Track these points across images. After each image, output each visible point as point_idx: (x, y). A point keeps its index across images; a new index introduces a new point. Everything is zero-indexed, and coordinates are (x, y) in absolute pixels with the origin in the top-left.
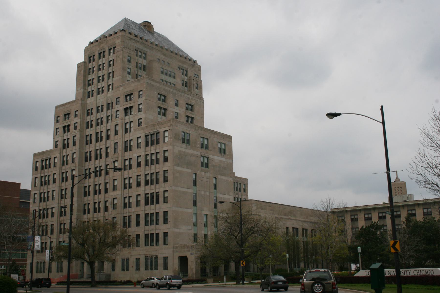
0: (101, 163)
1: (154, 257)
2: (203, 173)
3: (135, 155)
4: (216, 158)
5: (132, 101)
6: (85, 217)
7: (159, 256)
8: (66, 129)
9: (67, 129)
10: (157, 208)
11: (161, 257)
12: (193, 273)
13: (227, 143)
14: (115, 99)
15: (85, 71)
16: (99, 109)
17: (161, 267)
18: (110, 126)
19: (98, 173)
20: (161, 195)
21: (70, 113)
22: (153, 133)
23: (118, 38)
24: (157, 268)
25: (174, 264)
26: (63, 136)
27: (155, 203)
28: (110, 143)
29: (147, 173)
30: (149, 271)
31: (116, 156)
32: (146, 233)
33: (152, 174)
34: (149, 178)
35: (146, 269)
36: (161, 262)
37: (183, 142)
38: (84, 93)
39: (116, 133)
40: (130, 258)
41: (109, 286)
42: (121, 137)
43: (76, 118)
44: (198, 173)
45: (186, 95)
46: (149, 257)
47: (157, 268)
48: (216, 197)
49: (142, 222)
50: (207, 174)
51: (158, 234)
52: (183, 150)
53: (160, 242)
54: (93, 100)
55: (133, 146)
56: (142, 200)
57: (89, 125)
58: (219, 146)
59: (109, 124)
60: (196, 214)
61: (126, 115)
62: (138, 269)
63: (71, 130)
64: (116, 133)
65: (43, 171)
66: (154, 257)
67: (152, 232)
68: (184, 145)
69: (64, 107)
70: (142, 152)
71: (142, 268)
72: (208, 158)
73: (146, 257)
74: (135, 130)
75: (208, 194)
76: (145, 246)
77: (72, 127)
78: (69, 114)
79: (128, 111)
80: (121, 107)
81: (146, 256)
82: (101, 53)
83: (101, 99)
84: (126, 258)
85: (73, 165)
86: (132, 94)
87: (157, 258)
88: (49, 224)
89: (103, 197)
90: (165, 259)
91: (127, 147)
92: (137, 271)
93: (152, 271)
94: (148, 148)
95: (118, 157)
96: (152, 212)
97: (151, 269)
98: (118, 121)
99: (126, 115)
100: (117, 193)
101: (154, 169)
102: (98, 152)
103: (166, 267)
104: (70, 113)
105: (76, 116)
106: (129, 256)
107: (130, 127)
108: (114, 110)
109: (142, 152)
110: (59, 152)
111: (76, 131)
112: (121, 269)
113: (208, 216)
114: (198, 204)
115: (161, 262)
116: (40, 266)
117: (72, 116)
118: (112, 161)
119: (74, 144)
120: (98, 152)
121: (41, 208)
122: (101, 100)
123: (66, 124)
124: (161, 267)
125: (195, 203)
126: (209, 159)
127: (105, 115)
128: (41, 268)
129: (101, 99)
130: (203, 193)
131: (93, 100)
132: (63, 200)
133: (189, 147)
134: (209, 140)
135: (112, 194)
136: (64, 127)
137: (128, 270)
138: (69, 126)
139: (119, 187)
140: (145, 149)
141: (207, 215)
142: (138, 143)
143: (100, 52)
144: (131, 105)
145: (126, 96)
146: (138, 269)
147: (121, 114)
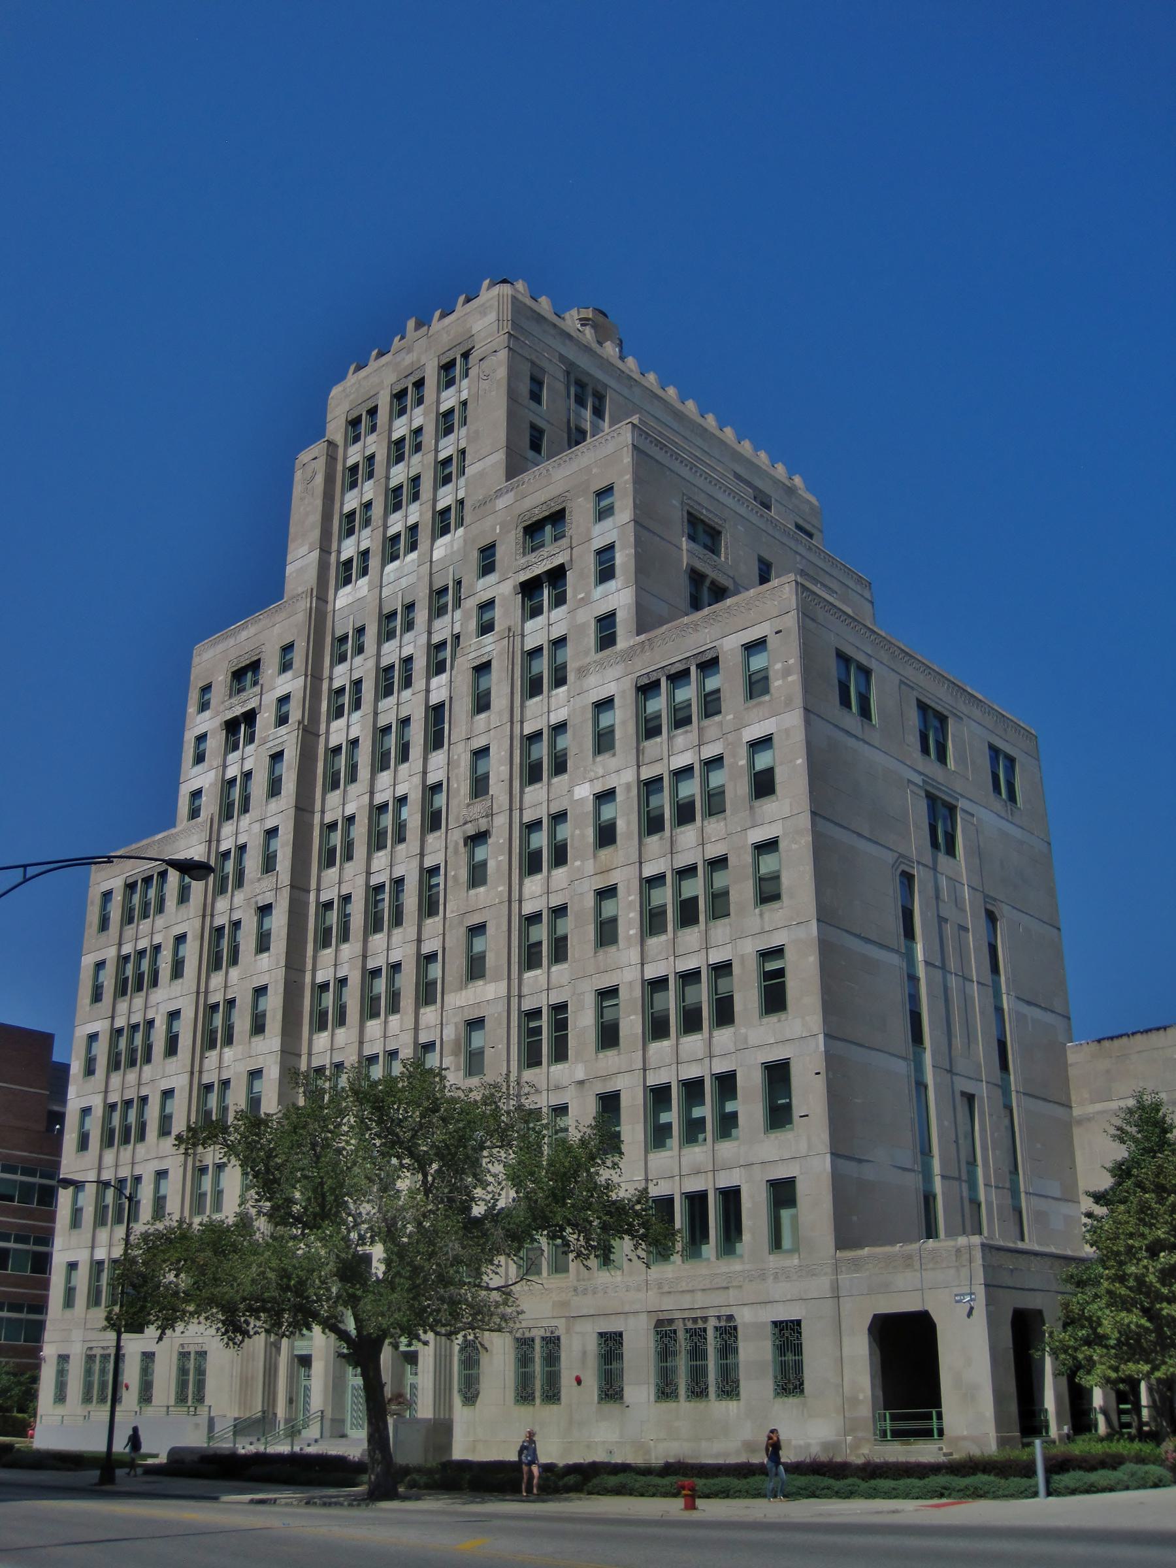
0: (400, 861)
1: (712, 1324)
3: (584, 792)
5: (564, 542)
6: (325, 1047)
7: (745, 1317)
10: (717, 1050)
15: (329, 479)
16: (391, 623)
17: (756, 1382)
19: (383, 905)
22: (680, 667)
24: (729, 1388)
25: (845, 1368)
26: (225, 767)
27: (702, 918)
29: (649, 871)
30: (684, 1406)
31: (480, 807)
32: (654, 1080)
33: (690, 977)
34: (670, 1001)
35: (666, 1392)
36: (755, 1353)
38: (323, 566)
40: (561, 1332)
42: (506, 717)
43: (289, 674)
46: (679, 1326)
47: (729, 1388)
49: (631, 1024)
51: (731, 1197)
53: (746, 1236)
56: (627, 912)
57: (345, 700)
62: (611, 1391)
65: (130, 931)
66: (712, 1324)
67: (694, 1185)
70: (623, 867)
71: (639, 1390)
73: (664, 1331)
77: (266, 718)
78: (255, 666)
80: (501, 588)
81: (659, 1323)
83: (403, 577)
84: (537, 1334)
85: (269, 881)
87: (729, 1332)
88: (147, 1172)
89: (354, 1037)
90: (788, 1335)
91: (541, 760)
92: (611, 1407)
93: (700, 1405)
94: (654, 746)
95: (490, 815)
96: (691, 1072)
97: (698, 1392)
98: (490, 646)
100: (488, 994)
101: (690, 844)
103: (790, 1381)
105: (285, 667)
106: (561, 1324)
109: (623, 867)
110: (205, 836)
111: (283, 730)
112: (510, 1394)
115: (755, 1353)
116: (103, 1371)
117: (269, 668)
121: (114, 1098)
122: (404, 583)
123: (238, 711)
128: (103, 1385)
129: (403, 577)
132: (213, 1055)
137: (552, 1395)
139: (495, 959)
140: (639, 752)
144: (557, 562)
146: (611, 1391)
147: (507, 612)
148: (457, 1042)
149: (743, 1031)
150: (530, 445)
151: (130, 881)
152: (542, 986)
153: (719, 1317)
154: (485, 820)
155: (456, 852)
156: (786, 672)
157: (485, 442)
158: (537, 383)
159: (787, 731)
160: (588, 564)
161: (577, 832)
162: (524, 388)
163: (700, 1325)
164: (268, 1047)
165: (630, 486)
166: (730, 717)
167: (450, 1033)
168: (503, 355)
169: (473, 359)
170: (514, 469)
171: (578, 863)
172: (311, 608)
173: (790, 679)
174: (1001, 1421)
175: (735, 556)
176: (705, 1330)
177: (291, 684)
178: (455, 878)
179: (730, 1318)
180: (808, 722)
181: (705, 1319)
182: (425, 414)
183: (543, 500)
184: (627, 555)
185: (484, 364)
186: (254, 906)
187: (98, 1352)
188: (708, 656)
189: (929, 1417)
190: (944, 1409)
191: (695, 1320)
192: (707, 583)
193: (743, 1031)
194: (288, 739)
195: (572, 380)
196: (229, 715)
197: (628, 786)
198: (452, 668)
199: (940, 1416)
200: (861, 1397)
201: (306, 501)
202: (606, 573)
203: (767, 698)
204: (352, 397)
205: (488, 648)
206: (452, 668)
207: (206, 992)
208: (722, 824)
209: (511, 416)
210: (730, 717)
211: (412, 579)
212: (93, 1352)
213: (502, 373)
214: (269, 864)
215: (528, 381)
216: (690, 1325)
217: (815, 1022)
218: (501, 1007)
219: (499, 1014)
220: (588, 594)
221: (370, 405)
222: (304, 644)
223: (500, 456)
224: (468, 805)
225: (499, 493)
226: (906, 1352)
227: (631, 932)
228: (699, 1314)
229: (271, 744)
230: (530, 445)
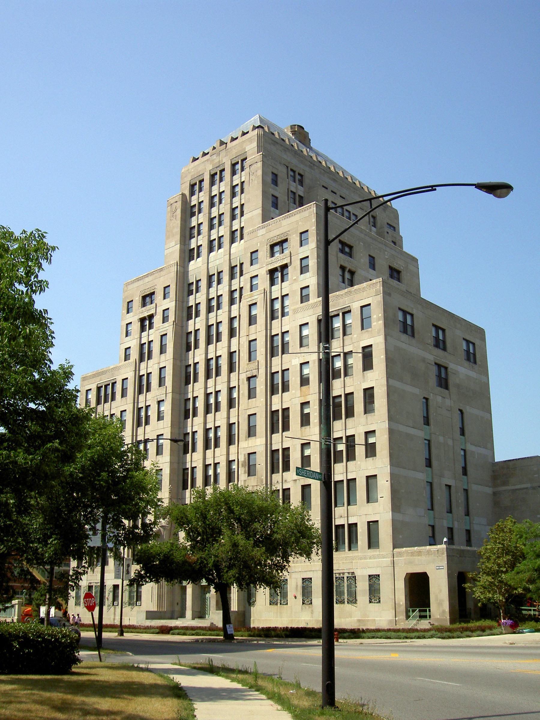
2: (439, 399)
4: (460, 370)
7: (358, 573)
8: (146, 323)
9: (147, 323)
11: (362, 574)
12: (444, 612)
13: (477, 342)
14: (249, 255)
15: (183, 211)
17: (363, 596)
18: (240, 310)
20: (360, 440)
21: (153, 293)
23: (250, 140)
25: (394, 592)
26: (141, 338)
28: (239, 345)
31: (253, 365)
36: (362, 586)
37: (405, 331)
39: (252, 320)
41: (452, 686)
44: (431, 397)
45: (388, 249)
48: (465, 451)
50: (448, 402)
52: (404, 346)
54: (200, 264)
55: (291, 345)
58: (465, 347)
59: (235, 307)
60: (431, 484)
61: (272, 282)
63: (155, 325)
64: (252, 320)
68: (404, 337)
69: (141, 282)
72: (446, 368)
74: (295, 311)
75: (450, 442)
76: (370, 547)
77: (157, 320)
79: (277, 274)
80: (261, 270)
82: (216, 174)
83: (219, 260)
86: (286, 240)
89: (225, 452)
90: (374, 579)
99: (272, 282)
102: (213, 362)
104: (153, 293)
107: (283, 307)
108: (246, 277)
111: (166, 324)
113: (453, 489)
114: (434, 463)
115: (362, 586)
118: (243, 377)
119: (163, 350)
120: (213, 362)
122: (218, 262)
123: (146, 314)
124: (363, 596)
125: (429, 463)
126: (449, 370)
127: (227, 289)
129: (219, 260)
130: (441, 439)
131: (200, 264)
133: (413, 341)
134: (447, 332)
135: (246, 445)
136: (142, 320)
138: (151, 317)
141: (449, 487)
142: (301, 338)
143: (212, 173)
144: (284, 262)
145: (272, 247)
147: (263, 281)
148: (245, 461)
149: (359, 463)
150: (273, 206)
151: (99, 386)
152: (278, 441)
153: (349, 573)
154: (255, 371)
155: (243, 383)
156: (379, 320)
157: (253, 199)
158: (275, 175)
159: (378, 343)
160: (296, 264)
161: (293, 379)
162: (269, 179)
163: (342, 575)
164: (314, 431)
165: (315, 232)
166: (355, 336)
167: (242, 458)
168: (260, 164)
169: (246, 164)
170: (266, 217)
171: (294, 391)
172: (177, 271)
173: (379, 322)
174: (451, 612)
175: (360, 261)
176: (343, 577)
177: (170, 304)
178: (243, 394)
179: (353, 573)
180: (386, 339)
181: (343, 573)
182: (226, 186)
183: (278, 234)
184: (314, 262)
185: (252, 167)
186: (156, 400)
187: (94, 585)
188: (347, 310)
189: (426, 611)
190: (431, 608)
191: (340, 574)
192: (347, 270)
193: (359, 463)
194: (169, 328)
195: (289, 169)
196: (142, 316)
197: (314, 361)
198: (240, 301)
199: (430, 610)
200: (401, 603)
201: (173, 221)
202: (304, 269)
203: (370, 329)
204: (192, 174)
205: (255, 297)
206: (240, 301)
207: (137, 436)
208: (352, 379)
209: (264, 192)
210: (355, 336)
211: (222, 261)
212: (92, 585)
213: (260, 173)
214: (161, 382)
215: (270, 175)
216: (338, 575)
217: (387, 461)
218: (263, 448)
219: (262, 451)
220: (298, 277)
221: (201, 179)
222: (175, 287)
223: (259, 211)
224: (248, 364)
225: (259, 228)
226: (418, 587)
227: (315, 421)
228: (341, 571)
229: (161, 330)
230: (273, 206)
